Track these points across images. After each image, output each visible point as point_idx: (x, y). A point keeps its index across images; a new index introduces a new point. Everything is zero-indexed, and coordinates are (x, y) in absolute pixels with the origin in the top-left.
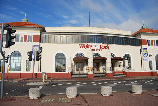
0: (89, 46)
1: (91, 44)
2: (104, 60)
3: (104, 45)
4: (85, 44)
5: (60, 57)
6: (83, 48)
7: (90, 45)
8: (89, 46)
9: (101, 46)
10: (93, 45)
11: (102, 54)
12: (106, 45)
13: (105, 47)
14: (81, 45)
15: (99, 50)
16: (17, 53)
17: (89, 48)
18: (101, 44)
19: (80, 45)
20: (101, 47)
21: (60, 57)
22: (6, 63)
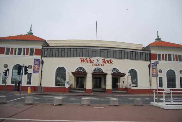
0: (91, 61)
1: (92, 59)
3: (106, 59)
4: (87, 58)
5: (61, 72)
6: (84, 62)
7: (92, 59)
9: (104, 61)
10: (95, 59)
12: (109, 59)
13: (108, 62)
14: (82, 60)
17: (90, 62)
18: (103, 58)
19: (81, 59)
20: (103, 61)
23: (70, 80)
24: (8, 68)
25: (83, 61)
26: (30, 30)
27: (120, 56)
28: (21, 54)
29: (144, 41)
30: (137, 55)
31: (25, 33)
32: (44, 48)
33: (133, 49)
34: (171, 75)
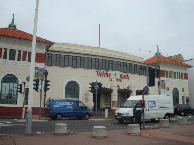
0: (108, 75)
1: (110, 72)
2: (108, 92)
4: (104, 71)
5: (72, 88)
6: (101, 76)
7: (109, 73)
8: (108, 74)
10: (112, 73)
11: (106, 83)
12: (125, 74)
13: (125, 77)
14: (99, 73)
15: (119, 81)
16: (11, 78)
17: (108, 77)
18: (121, 73)
19: (97, 72)
20: (120, 76)
21: (72, 88)
22: (19, 93)
23: (86, 99)
24: (166, 90)
25: (99, 75)
26: (12, 22)
27: (74, 64)
28: (14, 59)
29: (143, 53)
30: (130, 67)
31: (7, 26)
32: (49, 52)
33: (132, 61)
34: (176, 93)
